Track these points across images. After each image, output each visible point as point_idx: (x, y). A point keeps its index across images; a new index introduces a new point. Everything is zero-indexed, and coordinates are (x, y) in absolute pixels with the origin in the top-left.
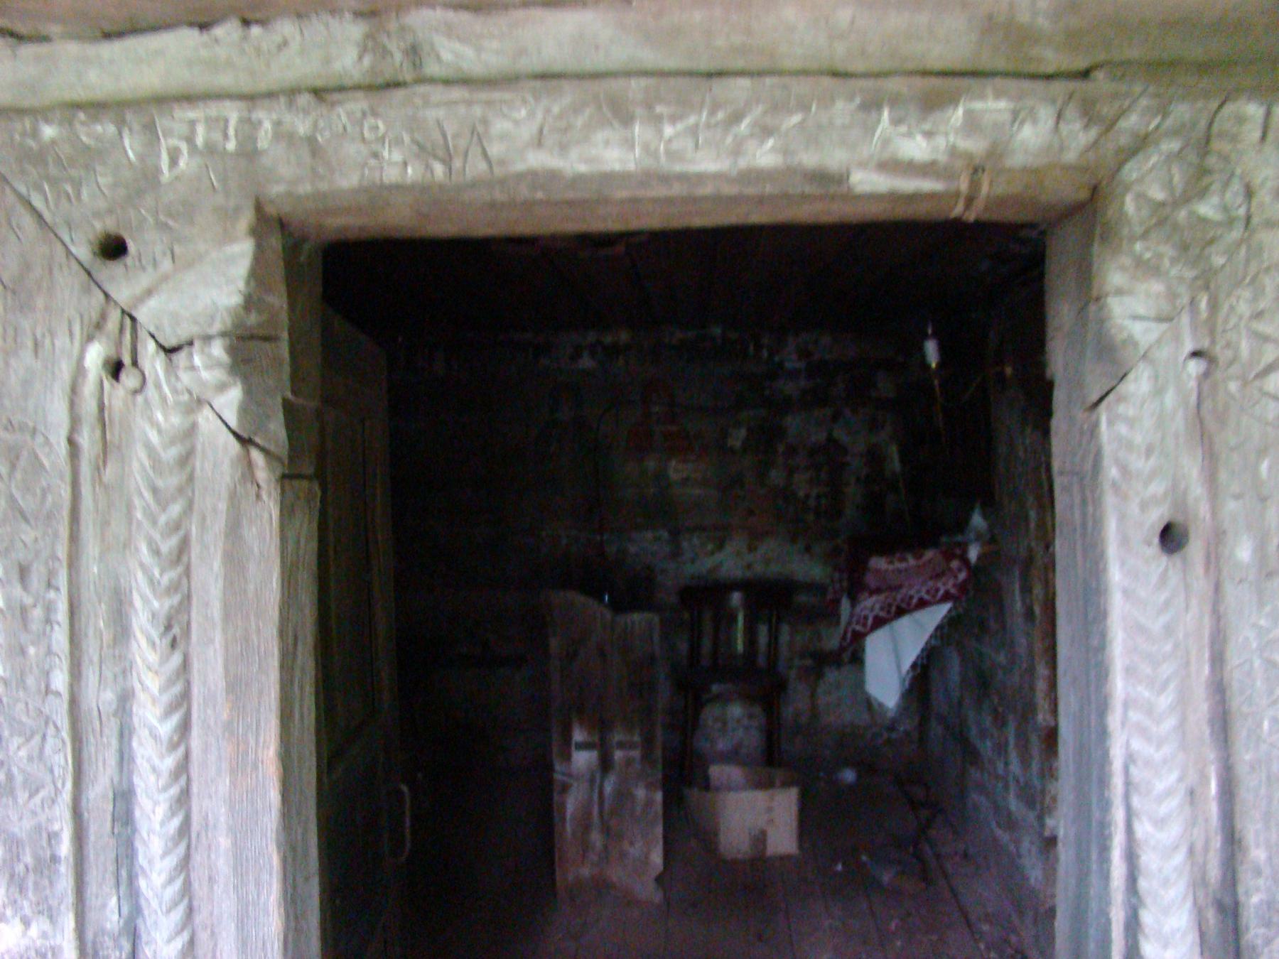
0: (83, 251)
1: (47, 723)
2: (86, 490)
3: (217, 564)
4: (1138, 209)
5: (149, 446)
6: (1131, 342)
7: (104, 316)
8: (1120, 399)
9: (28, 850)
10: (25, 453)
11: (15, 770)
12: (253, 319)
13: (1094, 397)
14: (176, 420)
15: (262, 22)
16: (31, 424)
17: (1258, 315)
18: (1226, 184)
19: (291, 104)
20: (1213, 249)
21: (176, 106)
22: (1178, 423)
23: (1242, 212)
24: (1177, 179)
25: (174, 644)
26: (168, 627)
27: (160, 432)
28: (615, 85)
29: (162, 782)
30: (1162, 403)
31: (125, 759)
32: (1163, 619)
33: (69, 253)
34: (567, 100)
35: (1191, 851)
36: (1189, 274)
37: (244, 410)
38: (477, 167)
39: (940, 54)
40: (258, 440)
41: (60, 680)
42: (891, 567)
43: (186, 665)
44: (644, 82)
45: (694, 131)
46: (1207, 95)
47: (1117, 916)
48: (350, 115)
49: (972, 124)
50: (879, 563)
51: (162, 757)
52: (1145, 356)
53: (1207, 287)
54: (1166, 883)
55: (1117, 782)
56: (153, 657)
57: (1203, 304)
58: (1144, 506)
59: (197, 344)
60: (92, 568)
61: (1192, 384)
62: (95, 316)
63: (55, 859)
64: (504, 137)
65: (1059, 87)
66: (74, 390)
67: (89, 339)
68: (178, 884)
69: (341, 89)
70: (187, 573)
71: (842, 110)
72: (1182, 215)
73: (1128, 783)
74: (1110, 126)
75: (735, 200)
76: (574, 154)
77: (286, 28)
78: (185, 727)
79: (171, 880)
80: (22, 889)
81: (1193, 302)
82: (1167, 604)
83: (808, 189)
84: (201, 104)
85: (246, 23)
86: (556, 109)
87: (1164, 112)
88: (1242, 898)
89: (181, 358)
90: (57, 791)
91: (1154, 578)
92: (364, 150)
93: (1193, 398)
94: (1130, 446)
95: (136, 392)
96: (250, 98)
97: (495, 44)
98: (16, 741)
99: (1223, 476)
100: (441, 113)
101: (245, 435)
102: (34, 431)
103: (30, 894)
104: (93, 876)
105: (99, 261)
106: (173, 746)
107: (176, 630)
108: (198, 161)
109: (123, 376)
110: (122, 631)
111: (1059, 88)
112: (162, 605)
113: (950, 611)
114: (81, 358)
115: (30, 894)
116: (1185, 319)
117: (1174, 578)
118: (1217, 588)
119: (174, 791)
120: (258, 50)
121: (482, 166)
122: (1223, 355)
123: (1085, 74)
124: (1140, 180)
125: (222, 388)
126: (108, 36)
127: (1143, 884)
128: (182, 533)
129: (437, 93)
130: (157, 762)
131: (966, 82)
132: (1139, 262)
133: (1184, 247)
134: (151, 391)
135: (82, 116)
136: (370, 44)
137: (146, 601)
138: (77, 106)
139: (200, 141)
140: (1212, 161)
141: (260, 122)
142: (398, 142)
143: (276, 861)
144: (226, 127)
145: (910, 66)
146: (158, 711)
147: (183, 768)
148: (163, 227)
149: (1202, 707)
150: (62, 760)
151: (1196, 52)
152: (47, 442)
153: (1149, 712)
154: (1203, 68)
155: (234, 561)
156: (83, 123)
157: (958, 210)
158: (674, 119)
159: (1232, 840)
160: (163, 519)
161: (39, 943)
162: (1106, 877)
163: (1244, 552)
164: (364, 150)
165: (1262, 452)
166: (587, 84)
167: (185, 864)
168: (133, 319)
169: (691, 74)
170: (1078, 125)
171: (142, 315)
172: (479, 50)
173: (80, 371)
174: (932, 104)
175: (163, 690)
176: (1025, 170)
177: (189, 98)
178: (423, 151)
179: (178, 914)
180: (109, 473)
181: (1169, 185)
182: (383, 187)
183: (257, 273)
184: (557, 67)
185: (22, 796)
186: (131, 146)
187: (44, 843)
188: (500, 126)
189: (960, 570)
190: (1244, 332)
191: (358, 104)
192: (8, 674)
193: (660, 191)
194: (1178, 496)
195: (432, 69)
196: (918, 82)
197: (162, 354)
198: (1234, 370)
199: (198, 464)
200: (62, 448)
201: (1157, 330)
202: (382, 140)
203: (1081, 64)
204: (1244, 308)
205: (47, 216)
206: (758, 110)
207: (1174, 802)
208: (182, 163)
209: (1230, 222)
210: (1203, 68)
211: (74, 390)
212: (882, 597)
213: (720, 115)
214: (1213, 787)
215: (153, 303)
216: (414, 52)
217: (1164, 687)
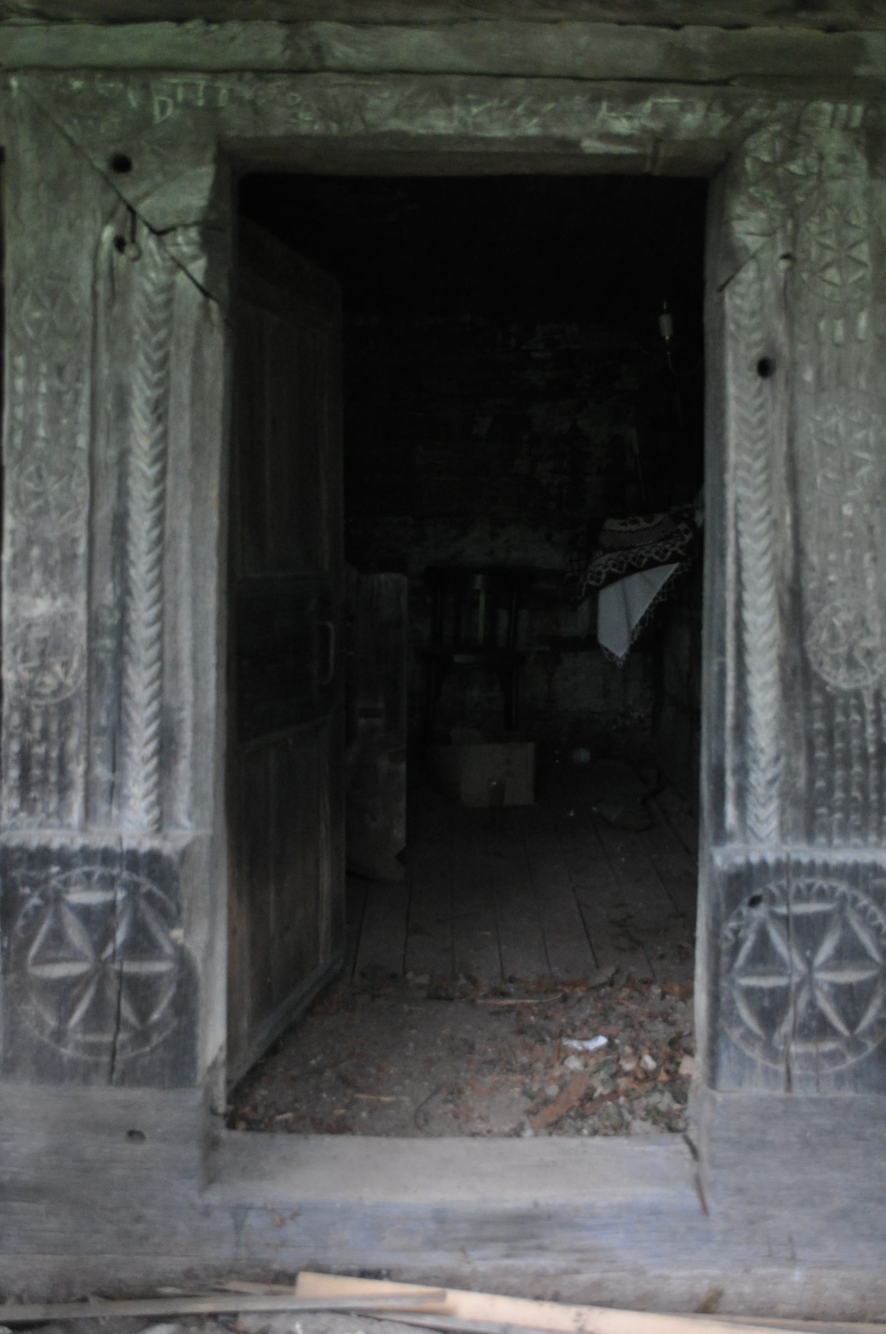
0: (101, 164)
2: (101, 320)
3: (187, 370)
6: (746, 248)
8: (739, 283)
12: (213, 216)
13: (722, 282)
14: (164, 278)
15: (219, 22)
17: (823, 233)
22: (772, 299)
23: (815, 170)
27: (153, 284)
29: (149, 506)
31: (123, 492)
32: (759, 415)
35: (774, 559)
36: (782, 207)
38: (358, 127)
39: (639, 67)
41: (82, 441)
42: (623, 528)
44: (461, 78)
50: (613, 524)
53: (792, 216)
54: (759, 576)
55: (730, 514)
56: (145, 426)
57: (790, 226)
58: (749, 347)
60: (105, 371)
61: (782, 275)
63: (75, 556)
66: (95, 256)
68: (155, 572)
69: (270, 71)
70: (168, 375)
71: (579, 101)
72: (780, 171)
73: (737, 516)
74: (738, 114)
77: (234, 27)
79: (150, 570)
81: (784, 226)
82: (762, 406)
87: (772, 107)
89: (168, 238)
93: (782, 284)
95: (135, 259)
96: (215, 72)
97: (368, 49)
98: (53, 479)
100: (335, 91)
108: (178, 112)
111: (710, 90)
113: (677, 570)
117: (767, 391)
118: (792, 398)
119: (155, 512)
122: (800, 256)
123: (725, 82)
125: (195, 258)
127: (745, 576)
129: (334, 78)
132: (752, 199)
133: (779, 191)
134: (147, 259)
135: (99, 76)
136: (290, 42)
137: (141, 389)
139: (180, 96)
140: (800, 138)
142: (308, 108)
146: (148, 460)
147: (161, 499)
149: (781, 470)
150: (82, 492)
153: (749, 469)
155: (197, 370)
158: (479, 103)
159: (799, 550)
160: (154, 340)
163: (809, 376)
165: (821, 315)
167: (159, 561)
171: (142, 208)
173: (98, 244)
174: (633, 99)
175: (152, 446)
178: (325, 115)
179: (154, 592)
180: (117, 309)
181: (772, 152)
183: (217, 187)
186: (133, 99)
188: (373, 102)
189: (686, 532)
191: (283, 82)
193: (468, 148)
194: (770, 342)
195: (329, 62)
196: (626, 85)
197: (153, 237)
201: (761, 240)
207: (762, 527)
208: (169, 112)
211: (95, 256)
212: (614, 555)
215: (148, 202)
216: (317, 49)
217: (757, 457)
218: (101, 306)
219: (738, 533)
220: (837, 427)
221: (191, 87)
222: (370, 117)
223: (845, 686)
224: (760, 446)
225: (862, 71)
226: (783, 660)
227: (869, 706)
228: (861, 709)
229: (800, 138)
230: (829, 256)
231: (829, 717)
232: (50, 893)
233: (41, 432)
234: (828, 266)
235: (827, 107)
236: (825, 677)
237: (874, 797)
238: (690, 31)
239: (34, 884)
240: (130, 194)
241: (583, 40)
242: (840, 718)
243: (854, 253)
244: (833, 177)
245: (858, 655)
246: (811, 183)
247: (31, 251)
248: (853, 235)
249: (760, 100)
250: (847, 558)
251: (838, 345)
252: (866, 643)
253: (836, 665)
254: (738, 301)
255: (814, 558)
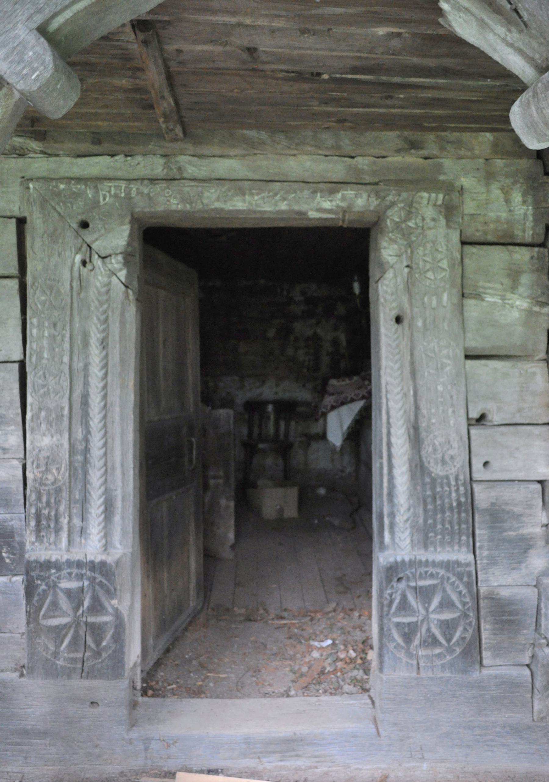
0: (75, 225)
1: (62, 372)
4: (391, 223)
5: (96, 287)
6: (388, 262)
7: (81, 246)
8: (385, 279)
9: (54, 413)
10: (55, 288)
11: (50, 387)
12: (130, 249)
13: (377, 279)
16: (57, 279)
17: (425, 255)
18: (417, 216)
19: (142, 184)
20: (412, 236)
21: (105, 181)
22: (401, 286)
24: (403, 215)
25: (104, 348)
26: (102, 343)
27: (100, 283)
28: (240, 183)
29: (99, 391)
30: (396, 280)
31: (86, 384)
32: (397, 342)
33: (70, 226)
34: (226, 187)
36: (405, 243)
37: (127, 277)
38: (199, 206)
40: (130, 286)
41: (66, 359)
43: (106, 356)
44: (249, 182)
45: (263, 198)
46: (412, 190)
47: (384, 431)
48: (161, 187)
49: (343, 198)
51: (99, 383)
52: (392, 267)
53: (410, 247)
55: (384, 390)
56: (97, 352)
59: (113, 256)
61: (406, 275)
62: (79, 246)
63: (62, 416)
64: (208, 197)
65: (369, 187)
67: (77, 253)
68: (103, 422)
71: (306, 193)
72: (404, 226)
73: (387, 391)
74: (384, 199)
75: (274, 219)
76: (229, 203)
77: (139, 158)
78: (106, 374)
79: (100, 422)
80: (51, 426)
81: (406, 252)
82: (398, 338)
83: (296, 216)
84: (113, 181)
85: (126, 156)
86: (223, 190)
88: (420, 424)
89: (107, 260)
90: (64, 394)
91: (393, 330)
92: (166, 199)
93: (406, 279)
94: (386, 292)
95: (92, 270)
97: (204, 168)
98: (51, 378)
99: (413, 301)
100: (188, 189)
101: (127, 285)
102: (59, 281)
103: (54, 427)
104: (74, 421)
105: (80, 229)
106: (103, 379)
107: (104, 344)
108: (112, 199)
109: (87, 265)
110: (86, 344)
112: (100, 336)
113: (365, 403)
114: (74, 259)
115: (54, 427)
116: (404, 256)
118: (412, 334)
119: (103, 393)
120: (130, 164)
121: (201, 206)
122: (414, 266)
123: (376, 184)
124: (392, 215)
125: (120, 270)
126: (79, 156)
128: (106, 314)
129: (188, 183)
130: (97, 384)
131: (343, 185)
132: (390, 239)
133: (403, 235)
134: (97, 270)
136: (166, 166)
137: (95, 334)
138: (71, 179)
139: (113, 193)
140: (413, 210)
141: (132, 188)
142: (175, 197)
143: (132, 417)
144: (121, 190)
145: (327, 180)
146: (99, 368)
147: (105, 387)
148: (101, 219)
150: (66, 384)
151: (410, 177)
152: (63, 285)
153: (392, 369)
154: (411, 182)
155: (123, 323)
156: (74, 185)
157: (340, 224)
158: (258, 194)
159: (417, 408)
160: (101, 309)
161: (56, 442)
162: (381, 419)
163: (420, 324)
164: (166, 199)
165: (425, 294)
166: (233, 182)
168: (90, 248)
169: (263, 181)
170: (374, 199)
171: (94, 246)
172: (200, 170)
173: (73, 263)
174: (332, 192)
175: (100, 362)
176: (359, 212)
177: (110, 179)
178: (183, 200)
180: (82, 295)
181: (400, 217)
182: (171, 211)
183: (131, 235)
184: (223, 177)
185: (52, 395)
186: (90, 194)
187: (59, 410)
188: (207, 194)
190: (421, 260)
191: (163, 185)
192: (49, 357)
193: (254, 216)
195: (185, 175)
197: (100, 259)
198: (418, 271)
199: (111, 294)
200: (68, 287)
202: (170, 196)
203: (376, 180)
204: (421, 253)
205: (62, 214)
206: (282, 192)
208: (107, 199)
209: (418, 227)
210: (411, 182)
213: (271, 194)
214: (412, 393)
215: (97, 243)
216: (179, 169)
217: (396, 363)
218: (75, 293)
219: (387, 400)
220: (434, 347)
221: (118, 187)
222: (205, 201)
223: (441, 474)
224: (397, 357)
225: (442, 178)
226: (411, 461)
227: (453, 483)
228: (449, 485)
229: (413, 210)
230: (428, 266)
231: (433, 489)
232: (51, 583)
233: (46, 355)
234: (428, 270)
235: (425, 195)
236: (431, 469)
237: (456, 527)
238: (359, 159)
239: (43, 579)
240: (88, 240)
241: (308, 164)
242: (439, 489)
243: (440, 264)
244: (429, 228)
245: (447, 458)
246: (419, 231)
247: (40, 267)
248: (440, 256)
249: (394, 192)
250: (441, 411)
251: (434, 309)
252: (451, 452)
253: (436, 463)
254: (385, 288)
255: (424, 411)
